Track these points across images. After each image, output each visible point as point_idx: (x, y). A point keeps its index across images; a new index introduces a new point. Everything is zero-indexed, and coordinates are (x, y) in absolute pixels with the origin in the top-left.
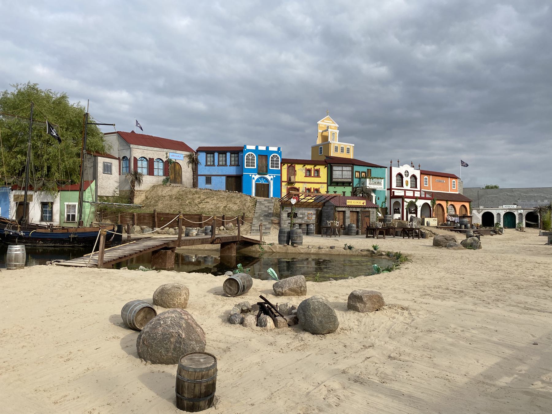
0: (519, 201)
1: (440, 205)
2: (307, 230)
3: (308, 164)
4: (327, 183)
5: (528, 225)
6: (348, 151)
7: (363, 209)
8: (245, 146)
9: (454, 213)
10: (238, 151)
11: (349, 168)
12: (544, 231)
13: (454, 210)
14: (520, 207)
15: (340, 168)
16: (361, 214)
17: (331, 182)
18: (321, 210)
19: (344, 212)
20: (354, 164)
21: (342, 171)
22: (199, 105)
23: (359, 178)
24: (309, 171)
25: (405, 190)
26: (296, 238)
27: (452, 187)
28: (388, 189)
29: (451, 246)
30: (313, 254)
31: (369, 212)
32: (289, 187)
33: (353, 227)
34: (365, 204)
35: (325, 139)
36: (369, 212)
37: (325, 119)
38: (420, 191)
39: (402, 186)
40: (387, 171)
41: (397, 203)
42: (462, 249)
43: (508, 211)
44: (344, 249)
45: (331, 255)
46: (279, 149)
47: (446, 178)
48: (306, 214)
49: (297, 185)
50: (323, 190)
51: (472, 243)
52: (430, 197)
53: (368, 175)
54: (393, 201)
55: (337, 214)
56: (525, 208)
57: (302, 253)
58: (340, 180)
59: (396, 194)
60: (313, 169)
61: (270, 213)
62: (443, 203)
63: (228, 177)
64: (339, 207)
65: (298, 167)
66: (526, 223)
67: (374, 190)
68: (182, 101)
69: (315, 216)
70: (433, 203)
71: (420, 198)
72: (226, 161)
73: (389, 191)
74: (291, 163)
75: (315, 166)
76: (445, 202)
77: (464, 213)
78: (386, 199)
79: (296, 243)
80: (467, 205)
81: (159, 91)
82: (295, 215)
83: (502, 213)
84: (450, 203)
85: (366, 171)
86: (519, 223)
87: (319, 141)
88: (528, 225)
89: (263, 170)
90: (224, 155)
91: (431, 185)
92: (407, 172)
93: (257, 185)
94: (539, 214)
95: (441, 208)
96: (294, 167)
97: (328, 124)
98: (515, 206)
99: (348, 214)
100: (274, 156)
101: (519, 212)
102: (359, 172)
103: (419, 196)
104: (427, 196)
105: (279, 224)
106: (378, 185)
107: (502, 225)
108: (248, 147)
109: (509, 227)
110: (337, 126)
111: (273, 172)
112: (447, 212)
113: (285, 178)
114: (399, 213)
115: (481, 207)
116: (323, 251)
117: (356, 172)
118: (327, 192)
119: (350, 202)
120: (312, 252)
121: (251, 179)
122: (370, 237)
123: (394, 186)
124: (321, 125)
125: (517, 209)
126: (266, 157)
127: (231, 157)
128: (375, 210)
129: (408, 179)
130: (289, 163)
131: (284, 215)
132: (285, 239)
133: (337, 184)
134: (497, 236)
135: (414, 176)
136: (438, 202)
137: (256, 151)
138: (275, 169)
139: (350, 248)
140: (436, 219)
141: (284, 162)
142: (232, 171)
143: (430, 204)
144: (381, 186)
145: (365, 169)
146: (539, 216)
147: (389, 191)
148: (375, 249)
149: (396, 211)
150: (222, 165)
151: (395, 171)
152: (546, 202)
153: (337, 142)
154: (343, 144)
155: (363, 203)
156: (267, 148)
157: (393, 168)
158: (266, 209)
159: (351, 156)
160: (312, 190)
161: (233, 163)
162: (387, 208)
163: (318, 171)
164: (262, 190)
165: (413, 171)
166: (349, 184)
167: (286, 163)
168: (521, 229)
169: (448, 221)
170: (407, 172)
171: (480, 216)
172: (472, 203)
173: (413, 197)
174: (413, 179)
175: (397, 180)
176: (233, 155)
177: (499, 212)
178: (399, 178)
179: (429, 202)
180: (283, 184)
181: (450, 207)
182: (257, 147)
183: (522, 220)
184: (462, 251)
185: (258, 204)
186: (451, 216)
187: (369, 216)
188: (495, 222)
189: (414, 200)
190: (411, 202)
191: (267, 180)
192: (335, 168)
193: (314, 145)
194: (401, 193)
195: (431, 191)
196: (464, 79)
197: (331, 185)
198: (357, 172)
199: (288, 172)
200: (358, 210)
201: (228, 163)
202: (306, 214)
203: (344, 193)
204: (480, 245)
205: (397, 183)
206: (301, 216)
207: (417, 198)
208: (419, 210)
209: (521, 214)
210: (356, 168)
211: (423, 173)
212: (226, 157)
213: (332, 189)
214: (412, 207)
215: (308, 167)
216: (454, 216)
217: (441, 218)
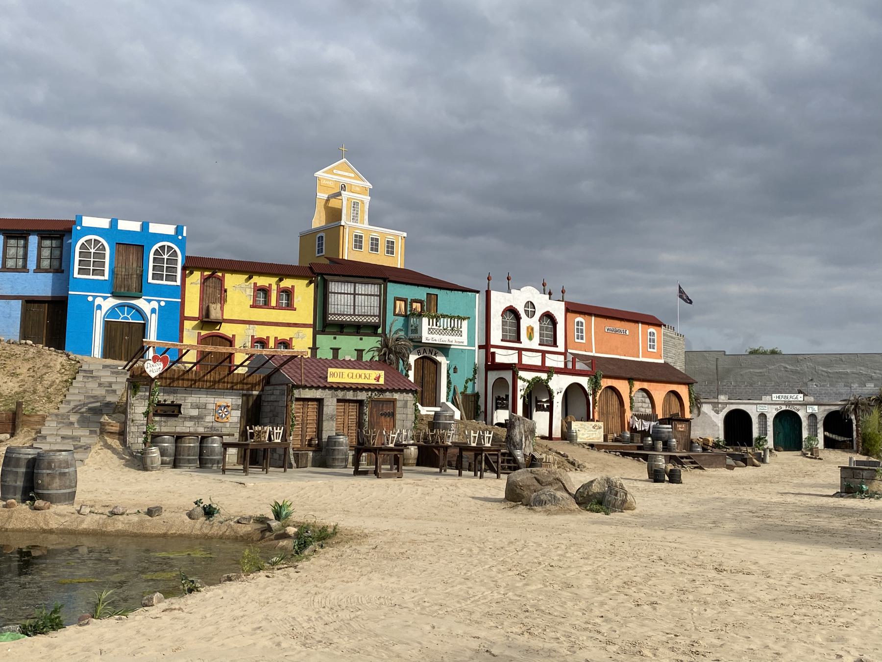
0: (813, 386)
1: (612, 388)
2: (201, 454)
3: (261, 274)
4: (314, 326)
5: (830, 444)
6: (390, 246)
7: (375, 395)
8: (78, 221)
9: (649, 411)
10: (59, 233)
11: (373, 289)
12: (864, 458)
13: (646, 402)
14: (811, 399)
15: (349, 288)
16: (372, 407)
17: (325, 324)
18: (259, 396)
19: (320, 401)
20: (386, 280)
21: (355, 294)
22: (128, 150)
23: (406, 316)
24: (265, 291)
25: (520, 351)
26: (46, 479)
27: (646, 346)
28: (480, 347)
29: (541, 503)
30: (86, 533)
31: (394, 401)
32: (203, 333)
33: (340, 444)
34: (382, 381)
35: (334, 215)
36: (394, 401)
37: (337, 168)
38: (564, 354)
39: (518, 340)
40: (479, 299)
41: (501, 381)
42: (571, 511)
43: (784, 408)
44: (190, 515)
45: (145, 536)
46: (179, 230)
47: (632, 324)
48: (211, 407)
49: (226, 330)
50: (302, 342)
51: (604, 494)
52: (586, 368)
53: (430, 309)
54: (493, 376)
55: (295, 406)
56: (825, 401)
57: (51, 532)
58: (348, 319)
59: (499, 359)
60: (274, 287)
61: (108, 404)
62: (622, 386)
63: (29, 302)
64: (305, 387)
65: (232, 281)
66: (825, 437)
67: (444, 349)
68: (87, 139)
69: (238, 413)
70: (595, 385)
71: (559, 371)
72: (25, 258)
73: (484, 351)
74: (214, 269)
75: (281, 280)
76: (627, 382)
77: (675, 409)
78: (475, 372)
79: (41, 497)
80: (683, 391)
81: (34, 114)
82: (173, 411)
83: (772, 413)
84: (638, 385)
85: (424, 297)
86: (809, 439)
87: (319, 221)
88: (830, 444)
89: (127, 286)
90: (22, 242)
91: (595, 340)
92: (530, 304)
93: (108, 326)
94: (853, 417)
95: (615, 397)
96: (221, 280)
97: (344, 180)
98: (800, 397)
99: (331, 406)
100: (162, 247)
101: (810, 410)
102: (405, 300)
103: (562, 365)
104: (580, 366)
105: (122, 434)
106: (455, 337)
107: (770, 443)
108: (88, 221)
109: (787, 448)
110: (369, 185)
111: (159, 291)
112: (631, 408)
113: (192, 308)
114: (506, 408)
115: (722, 398)
116: (120, 524)
117: (397, 299)
118: (314, 349)
119: (336, 376)
120: (84, 526)
121: (90, 309)
122: (365, 473)
123: (496, 337)
124: (324, 182)
125: (805, 404)
126: (141, 250)
127: (40, 247)
128: (410, 397)
129: (534, 322)
130: (207, 269)
131: (139, 408)
132: (20, 483)
133: (342, 328)
134: (749, 471)
135: (548, 316)
136: (605, 383)
137: (111, 232)
138: (164, 282)
139: (209, 512)
140: (601, 424)
141: (191, 265)
142: (42, 286)
143: (586, 386)
144: (462, 339)
145: (421, 293)
146: (854, 422)
147: (484, 351)
148: (278, 516)
149: (501, 404)
150: (15, 270)
151: (500, 301)
152: (871, 388)
153: (366, 225)
154: (377, 231)
155: (378, 379)
156: (145, 226)
157: (494, 294)
158: (100, 392)
159: (398, 261)
160: (272, 344)
161: (46, 264)
162: (477, 396)
163: (288, 293)
164: (125, 340)
165: (544, 303)
166: (371, 329)
167: (198, 268)
168: (813, 454)
169: (633, 430)
170: (530, 304)
171: (719, 420)
172: (695, 388)
173: (542, 369)
174: (547, 323)
175: (504, 323)
176: (47, 243)
177: (762, 410)
178: (510, 318)
179: (584, 381)
180: (188, 325)
181: (639, 397)
182: (114, 223)
183: (816, 430)
184: (579, 517)
185: (80, 377)
186: (640, 417)
187: (393, 415)
188: (755, 434)
189: (544, 376)
190: (537, 382)
191: (140, 312)
192: (334, 287)
193: (305, 229)
194: (511, 358)
195: (593, 354)
196: (728, 121)
197: (323, 332)
198: (400, 299)
199: (202, 292)
200: (362, 396)
201: (32, 264)
202: (211, 407)
203: (336, 351)
204: (624, 501)
205: (503, 330)
206: (195, 412)
207: (551, 371)
208: (558, 400)
209: (812, 416)
210: (394, 290)
211: (571, 309)
212: (26, 247)
213: (326, 342)
214: (539, 395)
215: (262, 281)
216: (647, 418)
217: (615, 423)
